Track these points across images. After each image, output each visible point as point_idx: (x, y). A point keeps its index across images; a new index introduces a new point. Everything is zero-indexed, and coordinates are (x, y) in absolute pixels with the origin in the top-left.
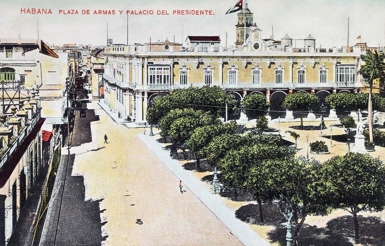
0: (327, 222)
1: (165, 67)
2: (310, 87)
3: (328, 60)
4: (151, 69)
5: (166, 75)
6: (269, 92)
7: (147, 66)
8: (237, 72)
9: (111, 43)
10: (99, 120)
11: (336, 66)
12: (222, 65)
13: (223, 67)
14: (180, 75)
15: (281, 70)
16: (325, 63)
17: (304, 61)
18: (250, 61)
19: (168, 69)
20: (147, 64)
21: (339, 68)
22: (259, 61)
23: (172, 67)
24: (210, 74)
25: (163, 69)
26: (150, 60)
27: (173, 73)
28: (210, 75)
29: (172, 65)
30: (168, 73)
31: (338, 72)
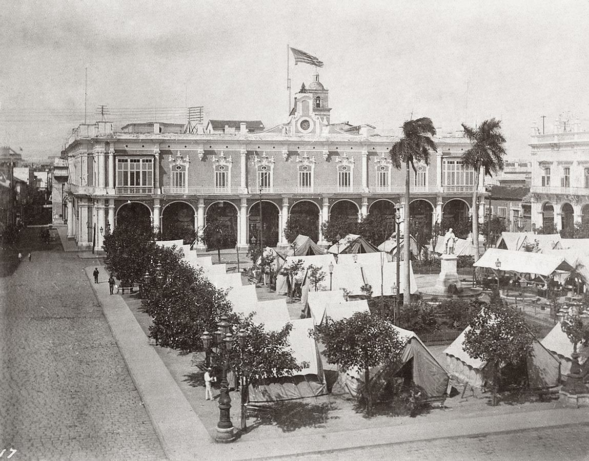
0: (414, 418)
1: (145, 158)
2: (398, 192)
3: (314, 148)
4: (119, 161)
5: (135, 170)
6: (326, 200)
7: (114, 157)
8: (272, 168)
9: (320, 107)
10: (414, 274)
11: (442, 158)
12: (366, 156)
13: (368, 159)
14: (215, 172)
15: (347, 164)
16: (308, 153)
17: (227, 150)
18: (165, 148)
19: (151, 161)
20: (114, 154)
21: (446, 162)
22: (269, 149)
23: (157, 157)
24: (385, 171)
25: (456, 162)
26: (122, 147)
27: (161, 167)
28: (308, 172)
29: (157, 154)
30: (466, 172)
31: (444, 169)
